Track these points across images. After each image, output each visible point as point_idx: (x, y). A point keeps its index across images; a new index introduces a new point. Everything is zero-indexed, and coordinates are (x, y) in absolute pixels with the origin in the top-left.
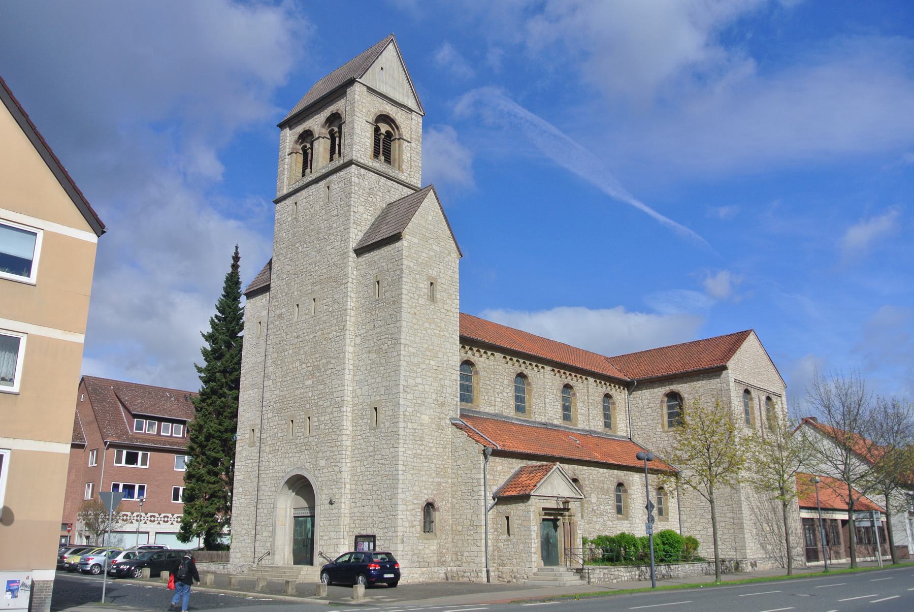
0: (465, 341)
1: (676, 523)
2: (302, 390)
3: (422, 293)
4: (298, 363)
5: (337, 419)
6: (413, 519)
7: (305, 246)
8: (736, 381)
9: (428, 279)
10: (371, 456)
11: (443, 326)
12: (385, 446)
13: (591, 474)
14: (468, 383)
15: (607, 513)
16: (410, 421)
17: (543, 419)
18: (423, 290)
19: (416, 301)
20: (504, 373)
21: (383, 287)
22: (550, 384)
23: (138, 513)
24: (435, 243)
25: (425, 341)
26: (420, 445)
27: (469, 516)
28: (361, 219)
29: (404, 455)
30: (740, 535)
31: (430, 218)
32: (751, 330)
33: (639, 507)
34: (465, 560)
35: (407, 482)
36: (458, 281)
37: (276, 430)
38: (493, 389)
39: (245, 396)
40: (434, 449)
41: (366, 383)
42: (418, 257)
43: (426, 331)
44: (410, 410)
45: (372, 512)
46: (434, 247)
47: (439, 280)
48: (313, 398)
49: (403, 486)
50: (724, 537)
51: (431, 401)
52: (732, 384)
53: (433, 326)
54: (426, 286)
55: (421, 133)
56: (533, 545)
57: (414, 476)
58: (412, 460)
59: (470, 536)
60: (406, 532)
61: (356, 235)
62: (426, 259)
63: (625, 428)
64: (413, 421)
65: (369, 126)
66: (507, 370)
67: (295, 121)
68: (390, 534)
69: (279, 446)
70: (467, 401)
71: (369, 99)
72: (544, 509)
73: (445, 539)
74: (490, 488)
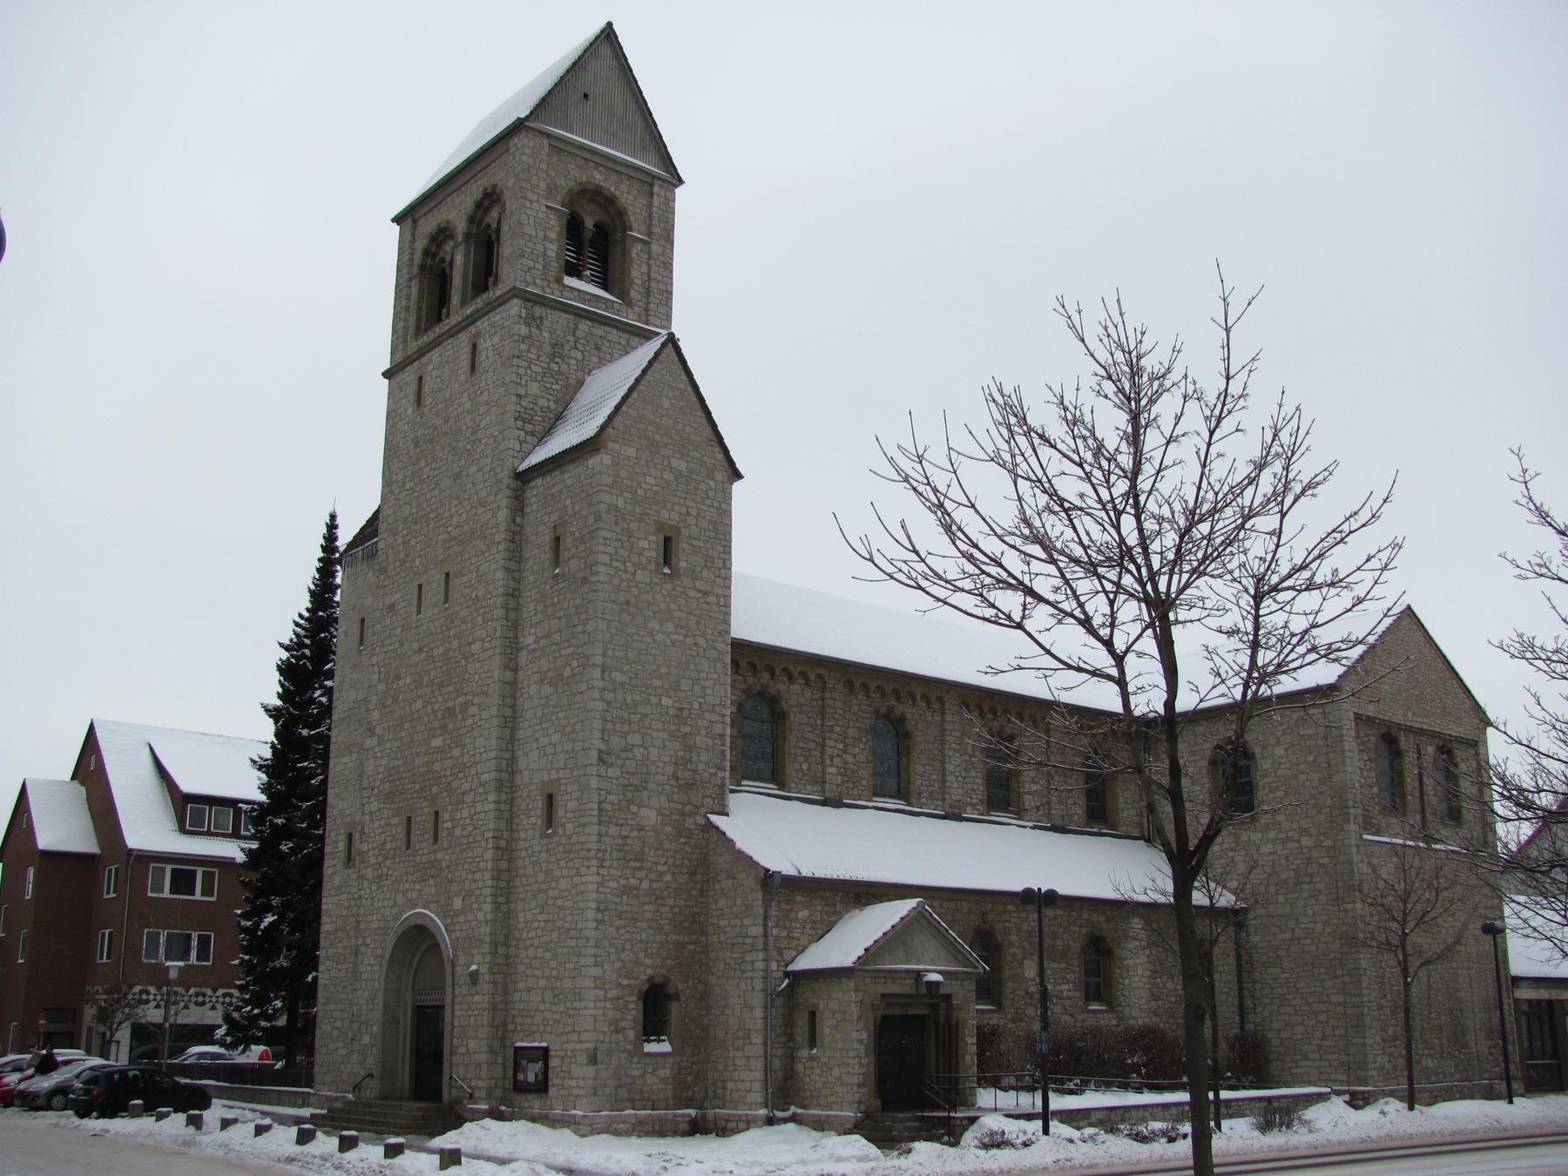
1: (1232, 1015)
2: (426, 759)
6: (619, 1015)
7: (434, 465)
10: (540, 891)
15: (1061, 998)
16: (614, 820)
21: (566, 550)
23: (226, 991)
24: (676, 455)
25: (651, 658)
29: (601, 889)
30: (1357, 1041)
31: (666, 403)
33: (1141, 985)
34: (728, 1098)
35: (606, 943)
37: (383, 836)
38: (819, 748)
39: (339, 768)
40: (668, 877)
41: (534, 745)
45: (543, 1002)
46: (675, 463)
48: (442, 773)
50: (1326, 1043)
51: (660, 778)
57: (621, 931)
58: (617, 900)
59: (738, 1050)
60: (603, 1042)
63: (1136, 819)
64: (620, 822)
67: (426, 209)
68: (570, 1046)
69: (388, 868)
72: (883, 995)
73: (693, 1055)
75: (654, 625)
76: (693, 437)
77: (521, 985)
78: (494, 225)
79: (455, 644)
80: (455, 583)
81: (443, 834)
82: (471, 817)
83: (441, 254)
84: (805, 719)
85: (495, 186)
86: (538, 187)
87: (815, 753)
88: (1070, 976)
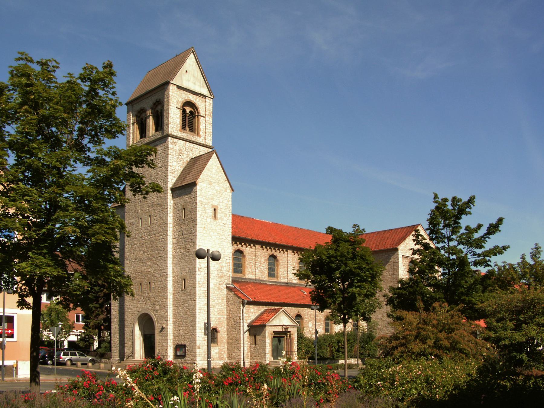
0: (236, 239)
4: (142, 252)
8: (403, 256)
9: (212, 207)
11: (222, 233)
12: (189, 299)
13: (309, 311)
14: (235, 262)
17: (285, 280)
19: (205, 220)
20: (262, 256)
22: (291, 260)
27: (235, 336)
31: (214, 170)
32: (419, 225)
36: (231, 206)
40: (216, 301)
43: (211, 237)
49: (199, 320)
52: (400, 259)
53: (216, 234)
55: (212, 110)
56: (267, 350)
65: (178, 110)
66: (263, 254)
67: (136, 102)
70: (238, 273)
71: (178, 93)
72: (274, 332)
74: (246, 321)
75: (212, 233)
76: (221, 180)
78: (159, 111)
83: (141, 117)
84: (250, 257)
85: (160, 99)
86: (174, 102)
87: (258, 271)
88: (321, 326)
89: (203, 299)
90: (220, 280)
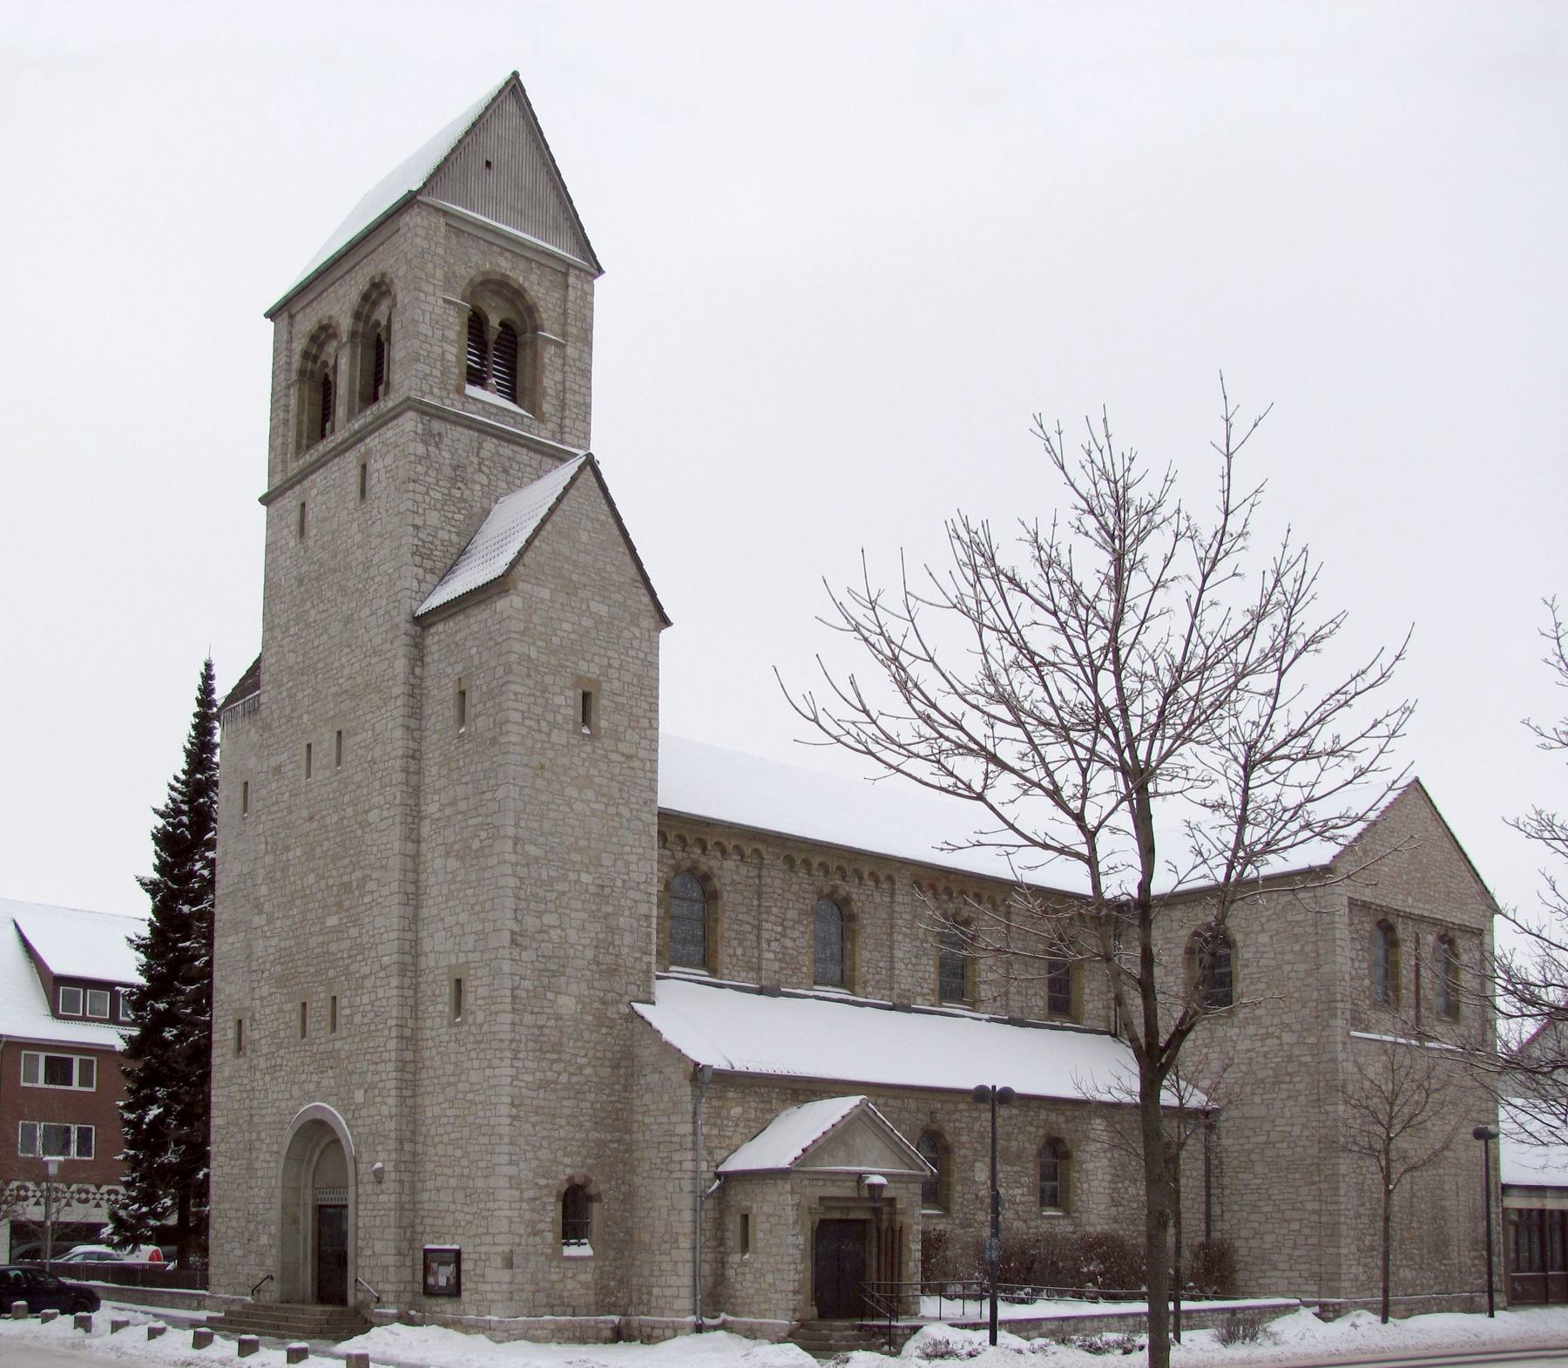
3: (560, 718)
4: (311, 879)
5: (384, 1002)
6: (536, 1217)
8: (1352, 903)
9: (576, 685)
10: (449, 1084)
12: (476, 1063)
13: (975, 1119)
15: (1014, 1203)
18: (563, 711)
19: (543, 737)
24: (596, 598)
26: (555, 1061)
28: (432, 543)
29: (515, 1083)
30: (1330, 1250)
33: (1101, 1190)
34: (654, 1304)
35: (521, 1141)
37: (276, 1023)
40: (588, 1071)
41: (440, 925)
42: (549, 631)
43: (569, 805)
44: (527, 984)
45: (454, 1202)
46: (594, 606)
47: (604, 685)
48: (339, 955)
50: (1297, 1253)
51: (581, 963)
53: (589, 794)
54: (570, 702)
58: (534, 1094)
60: (519, 1244)
61: (419, 582)
62: (573, 636)
63: (1102, 1012)
64: (536, 1010)
66: (795, 888)
68: (484, 1249)
75: (572, 792)
77: (430, 1184)
79: (350, 811)
80: (348, 743)
81: (341, 1021)
82: (372, 1003)
86: (434, 276)
88: (1025, 1180)
89: (529, 1064)
90: (605, 984)
